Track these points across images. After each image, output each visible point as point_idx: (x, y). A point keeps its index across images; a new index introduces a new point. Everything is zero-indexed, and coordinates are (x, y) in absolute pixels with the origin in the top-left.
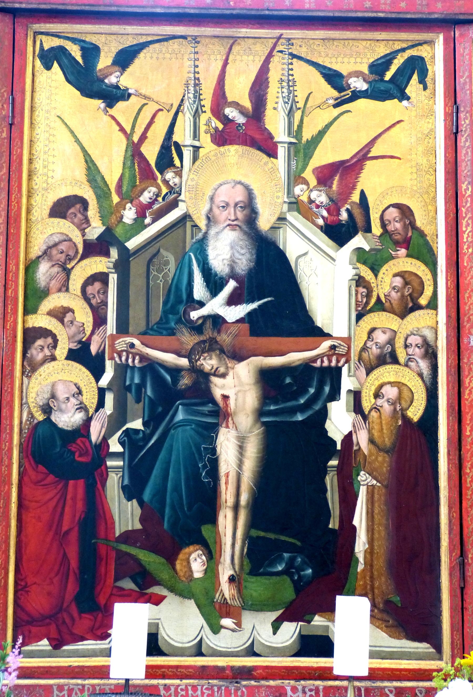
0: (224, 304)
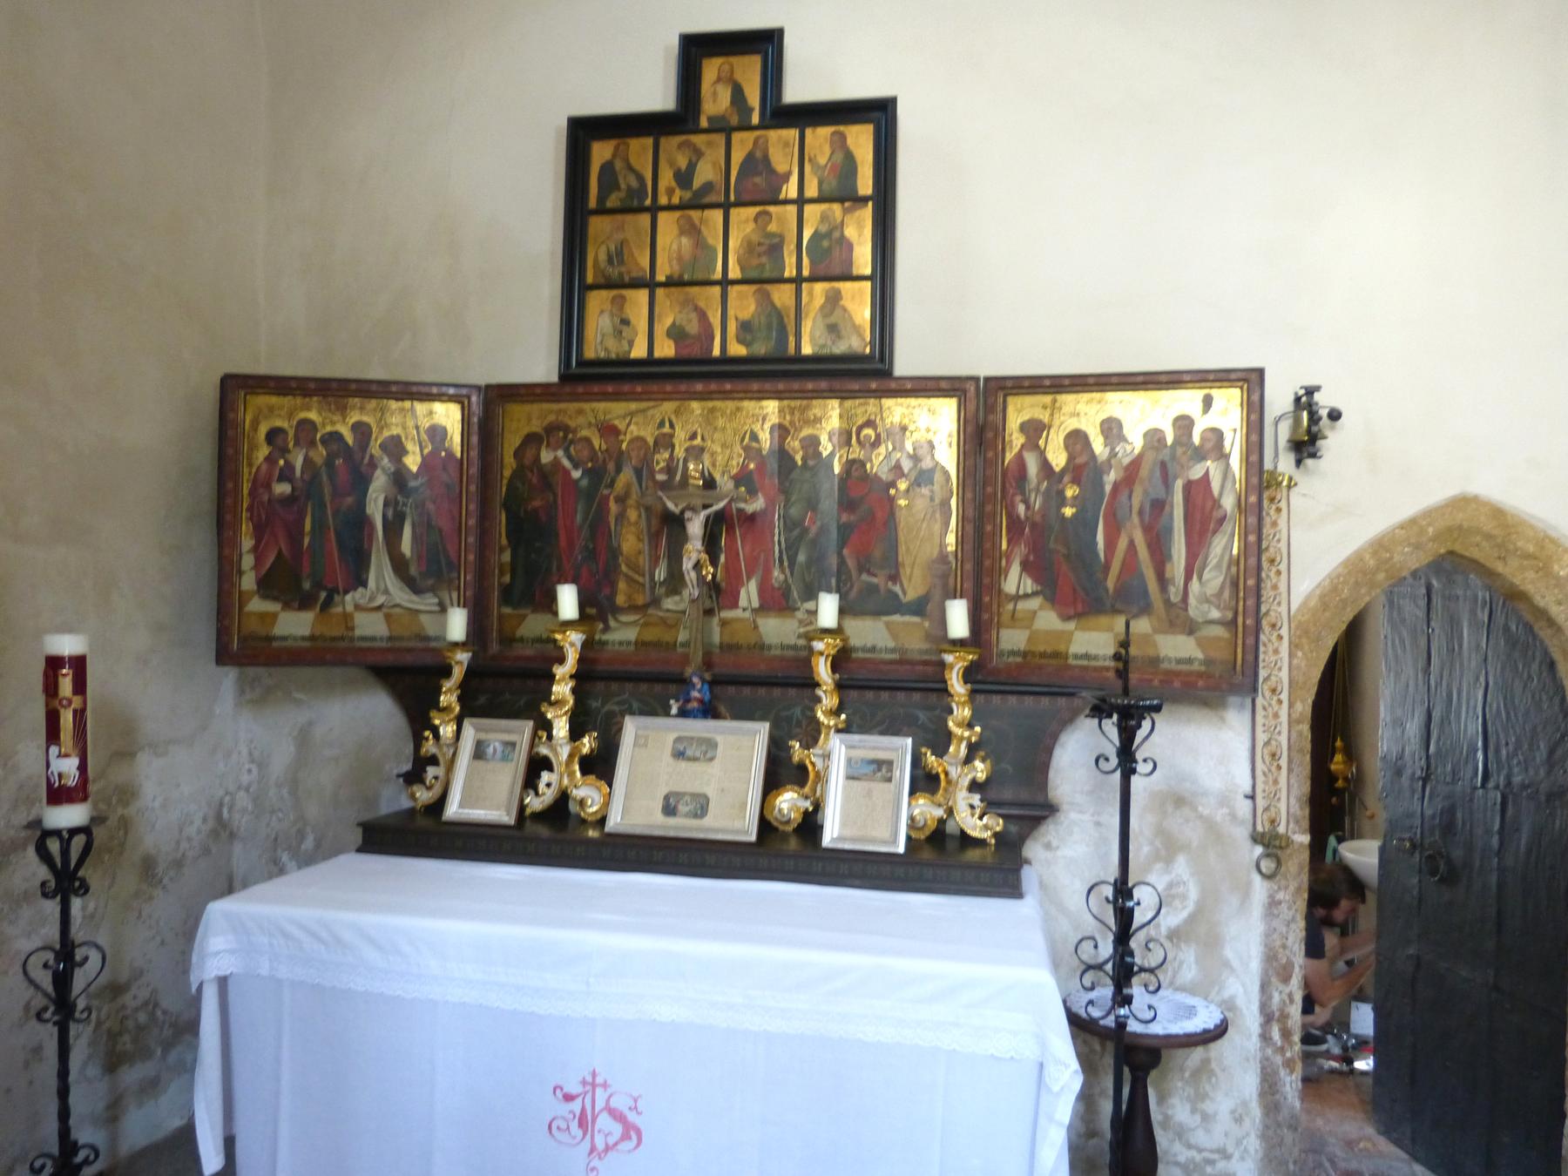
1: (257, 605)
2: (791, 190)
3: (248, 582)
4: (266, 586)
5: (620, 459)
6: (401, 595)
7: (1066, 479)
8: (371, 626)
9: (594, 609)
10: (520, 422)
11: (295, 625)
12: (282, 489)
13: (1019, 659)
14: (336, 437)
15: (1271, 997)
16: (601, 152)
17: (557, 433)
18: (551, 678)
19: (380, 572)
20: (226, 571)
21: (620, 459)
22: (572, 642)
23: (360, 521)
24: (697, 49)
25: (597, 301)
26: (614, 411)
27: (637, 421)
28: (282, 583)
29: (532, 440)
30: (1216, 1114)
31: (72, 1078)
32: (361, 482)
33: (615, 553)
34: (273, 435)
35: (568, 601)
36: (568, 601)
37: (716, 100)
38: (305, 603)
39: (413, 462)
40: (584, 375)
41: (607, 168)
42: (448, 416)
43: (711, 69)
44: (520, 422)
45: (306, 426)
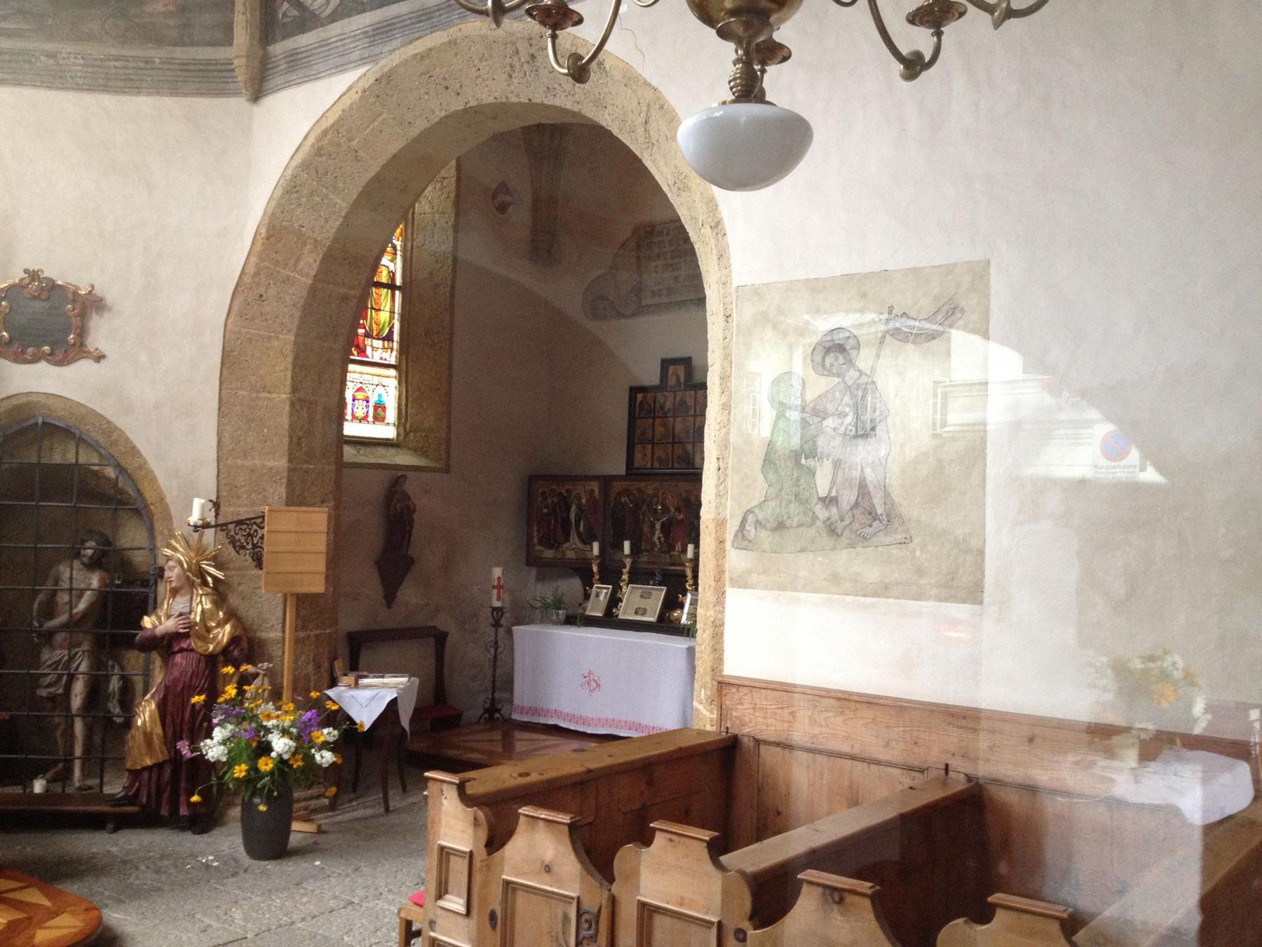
0: (110, 310)
1: (538, 548)
2: (692, 412)
3: (535, 540)
4: (541, 542)
5: (644, 501)
6: (580, 545)
7: (184, 748)
8: (571, 555)
9: (635, 550)
10: (617, 486)
11: (549, 554)
12: (545, 511)
13: (366, 681)
14: (561, 493)
15: (107, 678)
16: (640, 396)
17: (627, 492)
18: (622, 573)
19: (574, 537)
20: (530, 536)
21: (644, 501)
22: (628, 562)
23: (567, 520)
24: (666, 363)
25: (638, 447)
26: (642, 485)
27: (650, 488)
28: (548, 542)
29: (619, 494)
30: (969, 778)
31: (881, 768)
32: (568, 509)
33: (641, 530)
34: (543, 493)
35: (627, 545)
36: (627, 545)
37: (672, 381)
38: (550, 547)
39: (584, 501)
40: (632, 471)
41: (641, 402)
42: (595, 486)
43: (671, 369)
44: (617, 486)
45: (552, 490)
